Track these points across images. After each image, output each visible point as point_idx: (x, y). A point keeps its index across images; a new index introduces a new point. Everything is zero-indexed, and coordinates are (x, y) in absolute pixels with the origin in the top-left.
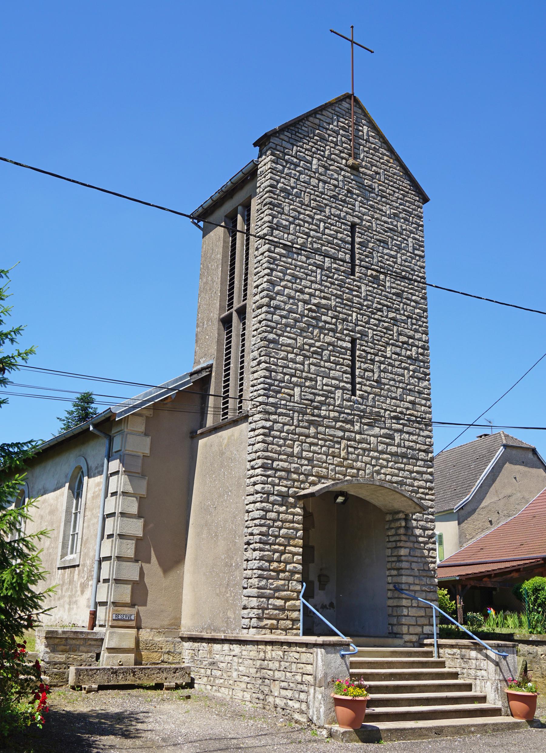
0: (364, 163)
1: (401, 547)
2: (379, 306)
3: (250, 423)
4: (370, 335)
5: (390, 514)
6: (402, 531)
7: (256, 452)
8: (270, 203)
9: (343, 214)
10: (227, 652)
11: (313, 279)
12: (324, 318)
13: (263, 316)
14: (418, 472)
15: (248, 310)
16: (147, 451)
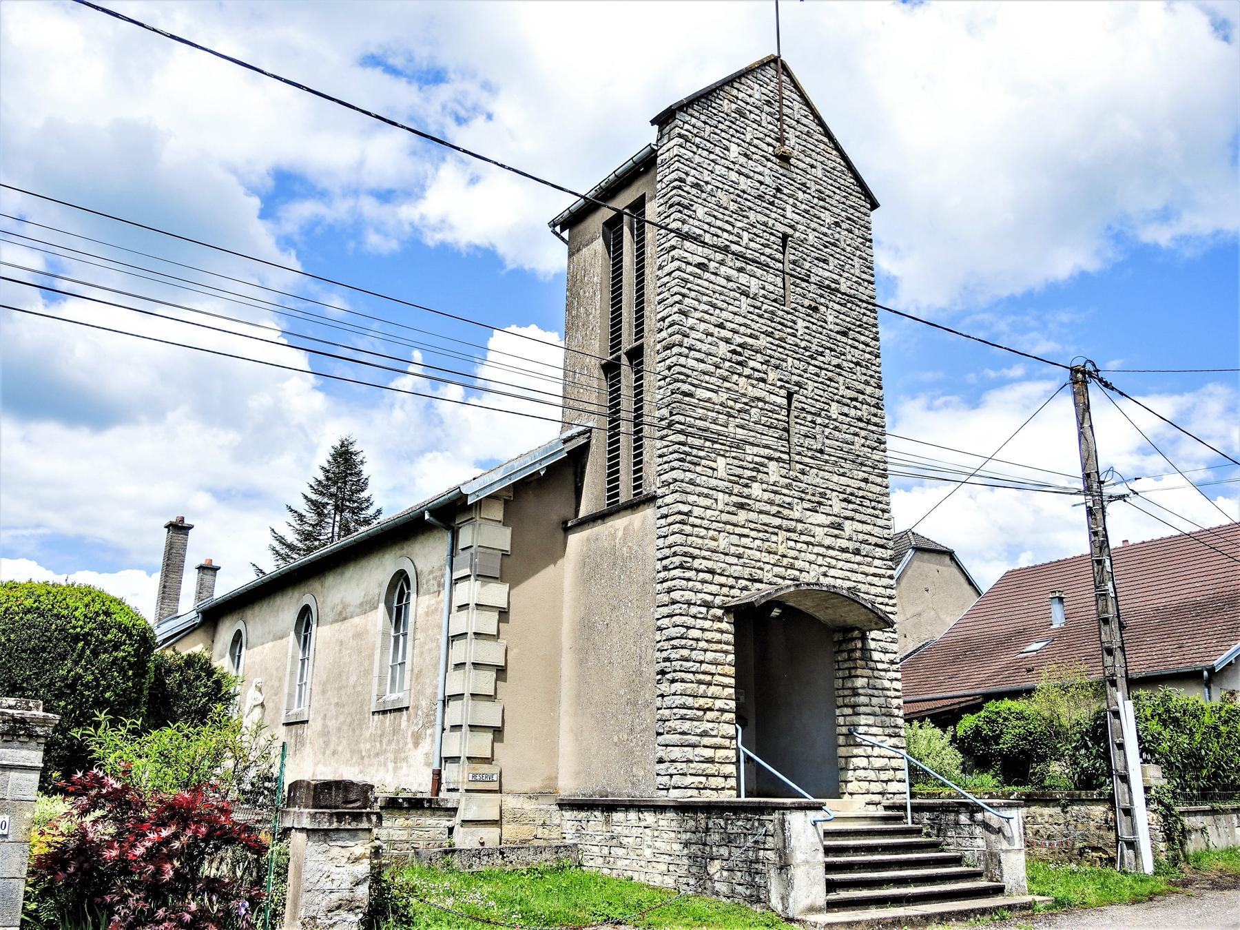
0: (795, 153)
1: (857, 676)
2: (821, 349)
3: (659, 507)
4: (810, 389)
5: (839, 631)
6: (858, 654)
7: (670, 547)
8: (678, 204)
9: (771, 222)
10: (634, 822)
11: (737, 310)
12: (751, 364)
13: (674, 359)
14: (874, 575)
15: (647, 351)
16: (508, 548)
